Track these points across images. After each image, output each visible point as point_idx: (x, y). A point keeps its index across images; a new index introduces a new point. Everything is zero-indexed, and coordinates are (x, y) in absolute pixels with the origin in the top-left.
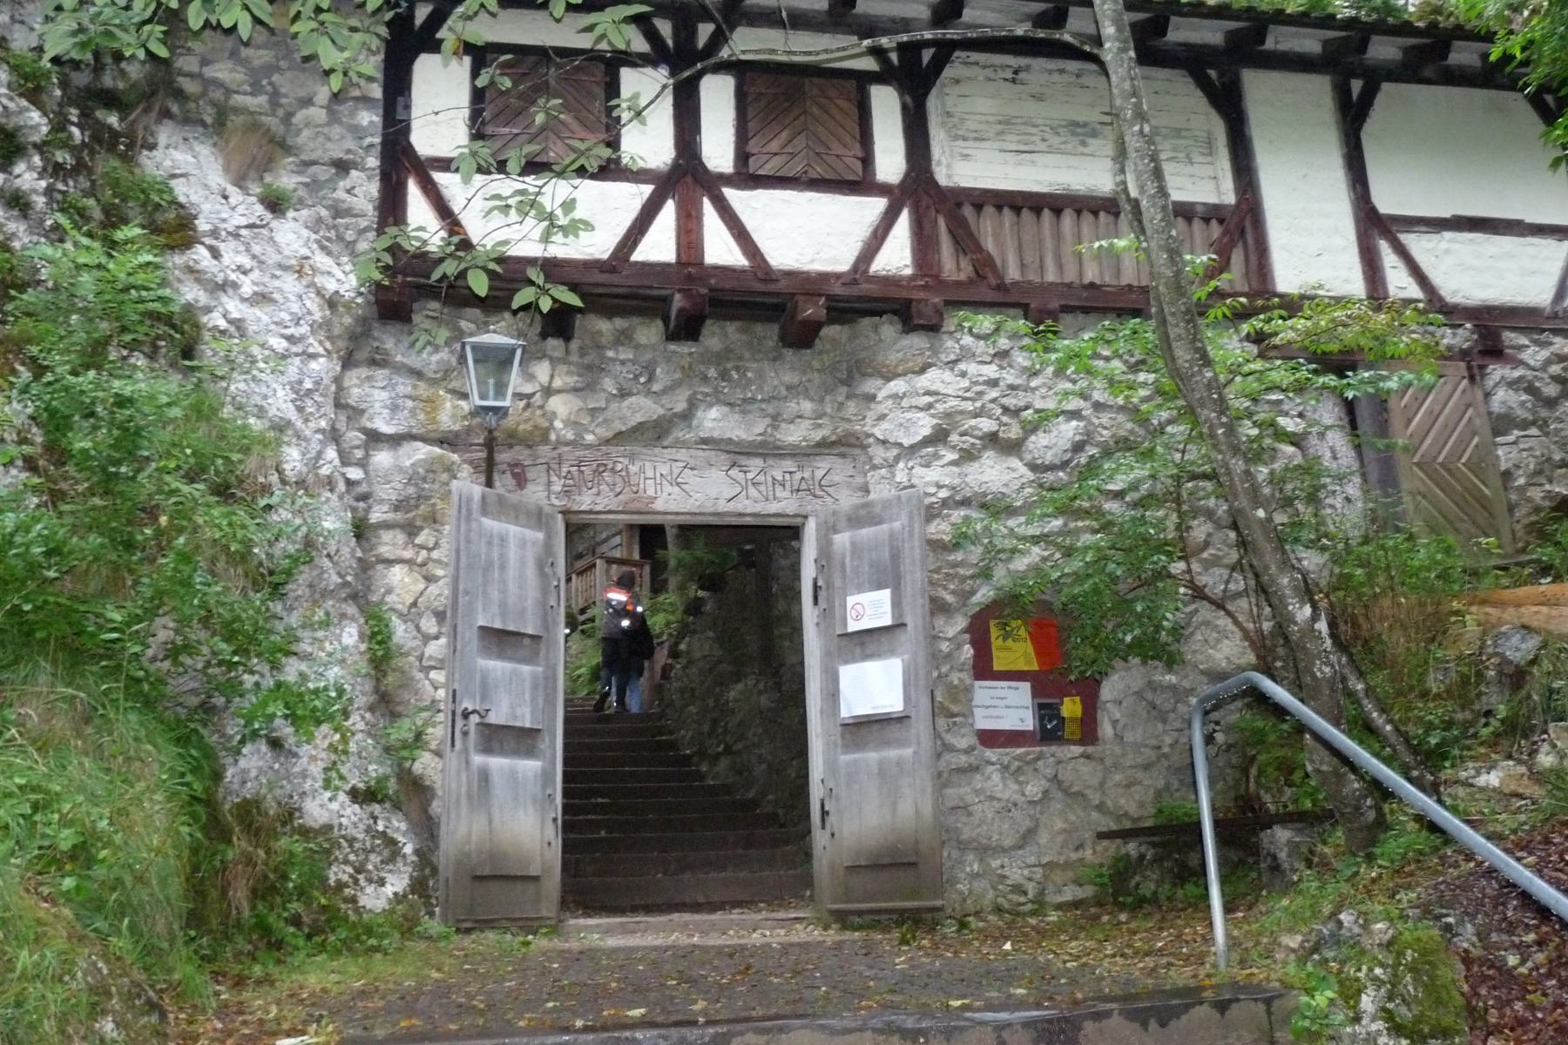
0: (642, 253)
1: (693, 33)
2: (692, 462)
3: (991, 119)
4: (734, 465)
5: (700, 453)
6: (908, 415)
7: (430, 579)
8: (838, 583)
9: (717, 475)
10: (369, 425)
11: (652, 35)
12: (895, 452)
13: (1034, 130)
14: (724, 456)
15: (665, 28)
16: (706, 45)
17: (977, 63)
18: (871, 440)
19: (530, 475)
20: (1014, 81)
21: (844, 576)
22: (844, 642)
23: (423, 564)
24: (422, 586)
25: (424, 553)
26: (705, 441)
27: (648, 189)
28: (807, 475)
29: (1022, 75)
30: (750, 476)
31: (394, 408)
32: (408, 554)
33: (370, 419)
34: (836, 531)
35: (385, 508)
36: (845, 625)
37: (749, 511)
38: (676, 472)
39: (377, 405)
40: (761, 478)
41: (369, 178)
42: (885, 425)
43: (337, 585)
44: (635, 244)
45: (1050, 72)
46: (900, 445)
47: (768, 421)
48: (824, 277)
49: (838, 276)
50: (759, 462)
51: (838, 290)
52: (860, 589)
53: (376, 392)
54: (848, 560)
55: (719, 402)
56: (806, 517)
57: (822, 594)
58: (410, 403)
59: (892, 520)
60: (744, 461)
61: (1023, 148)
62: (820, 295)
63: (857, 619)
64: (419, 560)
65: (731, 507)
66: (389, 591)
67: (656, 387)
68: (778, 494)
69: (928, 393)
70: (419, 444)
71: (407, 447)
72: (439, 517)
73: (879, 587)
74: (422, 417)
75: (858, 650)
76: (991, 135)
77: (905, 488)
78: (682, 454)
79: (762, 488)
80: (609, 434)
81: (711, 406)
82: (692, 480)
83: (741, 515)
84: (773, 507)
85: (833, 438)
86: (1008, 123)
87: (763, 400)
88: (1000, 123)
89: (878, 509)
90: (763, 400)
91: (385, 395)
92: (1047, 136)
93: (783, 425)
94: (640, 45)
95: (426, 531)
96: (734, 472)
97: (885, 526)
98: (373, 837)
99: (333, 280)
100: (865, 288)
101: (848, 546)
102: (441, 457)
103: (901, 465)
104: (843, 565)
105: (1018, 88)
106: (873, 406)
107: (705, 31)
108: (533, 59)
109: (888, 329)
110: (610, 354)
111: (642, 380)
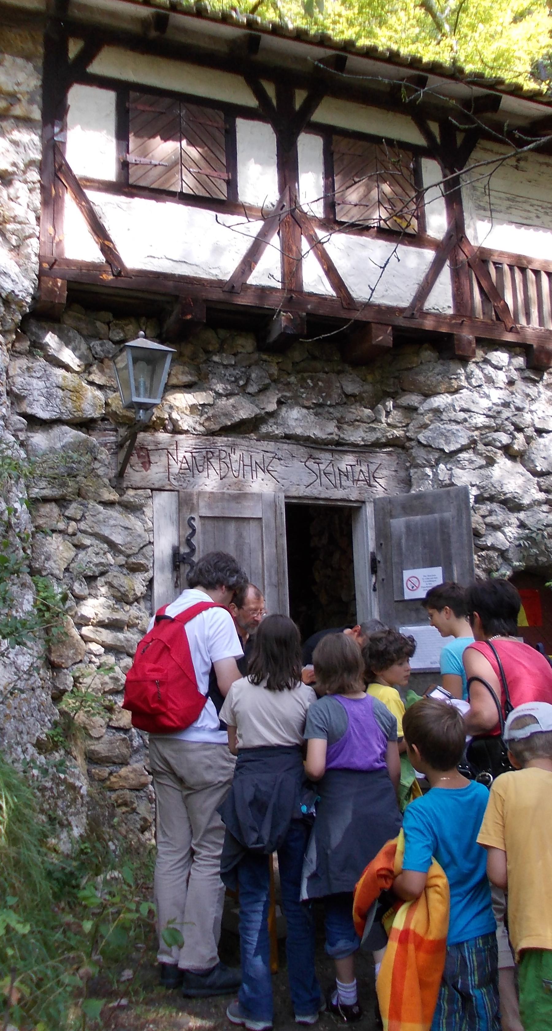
0: (255, 279)
1: (291, 98)
2: (280, 454)
3: (503, 195)
4: (311, 457)
5: (285, 446)
6: (448, 427)
7: (79, 547)
8: (395, 559)
9: (298, 465)
10: (29, 411)
11: (260, 94)
12: (437, 455)
13: (530, 208)
14: (302, 450)
15: (270, 90)
16: (301, 108)
17: (492, 151)
18: (413, 443)
19: (152, 459)
20: (517, 168)
21: (400, 554)
22: (401, 606)
23: (74, 534)
24: (73, 554)
25: (73, 523)
26: (288, 437)
27: (257, 226)
28: (364, 468)
29: (522, 164)
30: (322, 467)
31: (49, 396)
32: (61, 526)
33: (30, 405)
34: (392, 517)
35: (43, 484)
36: (403, 594)
37: (323, 496)
38: (267, 461)
39: (36, 393)
40: (330, 469)
41: (31, 190)
42: (427, 433)
43: (23, 558)
44: (251, 270)
45: (541, 164)
46: (442, 450)
47: (335, 423)
48: (391, 310)
49: (401, 310)
50: (328, 456)
51: (401, 322)
52: (415, 566)
53: (35, 381)
54: (403, 541)
55: (297, 404)
56: (364, 502)
57: (381, 567)
58: (60, 393)
59: (442, 511)
60: (317, 454)
61: (525, 221)
62: (388, 325)
63: (412, 590)
64: (70, 530)
65: (308, 492)
66: (48, 559)
67: (252, 389)
68: (344, 483)
69: (463, 410)
70: (66, 428)
71: (57, 430)
72: (83, 492)
73: (432, 565)
74: (70, 405)
75: (413, 614)
76: (503, 208)
77: (446, 486)
78: (270, 446)
79: (332, 478)
80: (217, 427)
81: (291, 407)
82: (279, 468)
83: (317, 499)
84: (339, 494)
85: (384, 440)
86: (513, 200)
87: (330, 406)
88: (508, 199)
89: (429, 501)
90: (330, 406)
91: (41, 384)
92: (540, 215)
93: (345, 426)
94: (252, 102)
95: (74, 505)
96: (310, 463)
97: (436, 515)
98: (58, 785)
99: (8, 280)
100: (244, 300)
101: (403, 530)
102: (86, 441)
103: (442, 466)
104: (399, 544)
105: (519, 174)
106: (415, 416)
107: (300, 97)
108: (168, 101)
109: (427, 354)
110: (216, 359)
111: (241, 383)
